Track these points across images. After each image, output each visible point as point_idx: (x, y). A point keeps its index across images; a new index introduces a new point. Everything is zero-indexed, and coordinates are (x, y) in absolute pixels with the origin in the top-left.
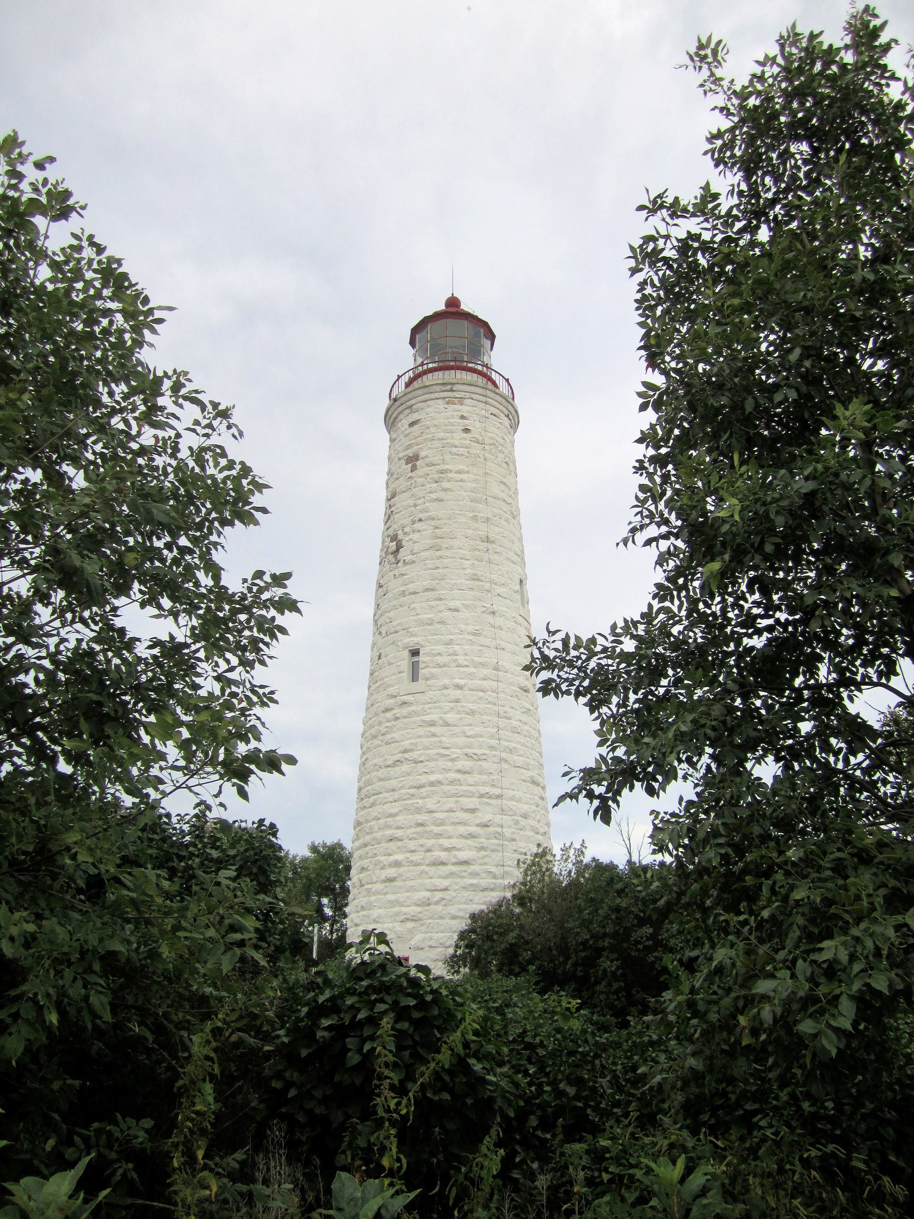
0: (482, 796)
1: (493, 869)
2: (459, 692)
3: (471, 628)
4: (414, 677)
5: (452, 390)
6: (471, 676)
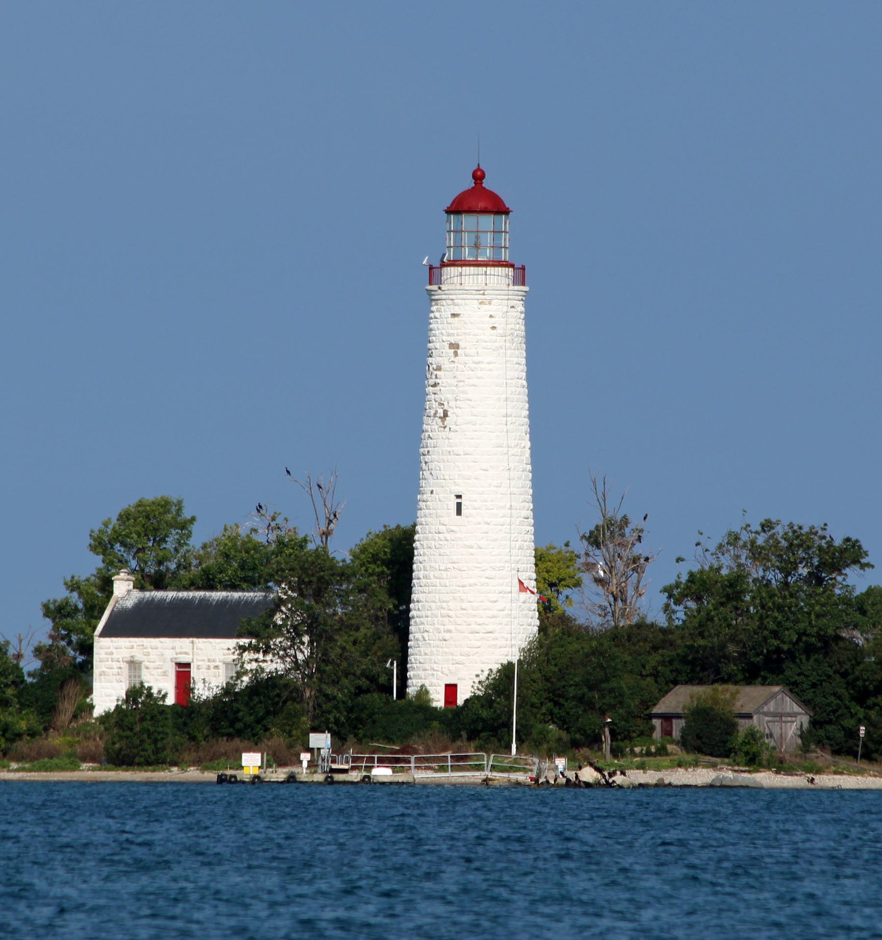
1: (505, 636)
2: (487, 526)
5: (484, 294)
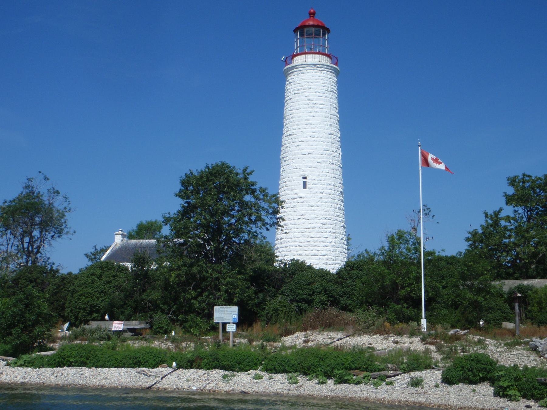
0: (330, 233)
3: (325, 170)
4: (305, 187)
6: (326, 189)
